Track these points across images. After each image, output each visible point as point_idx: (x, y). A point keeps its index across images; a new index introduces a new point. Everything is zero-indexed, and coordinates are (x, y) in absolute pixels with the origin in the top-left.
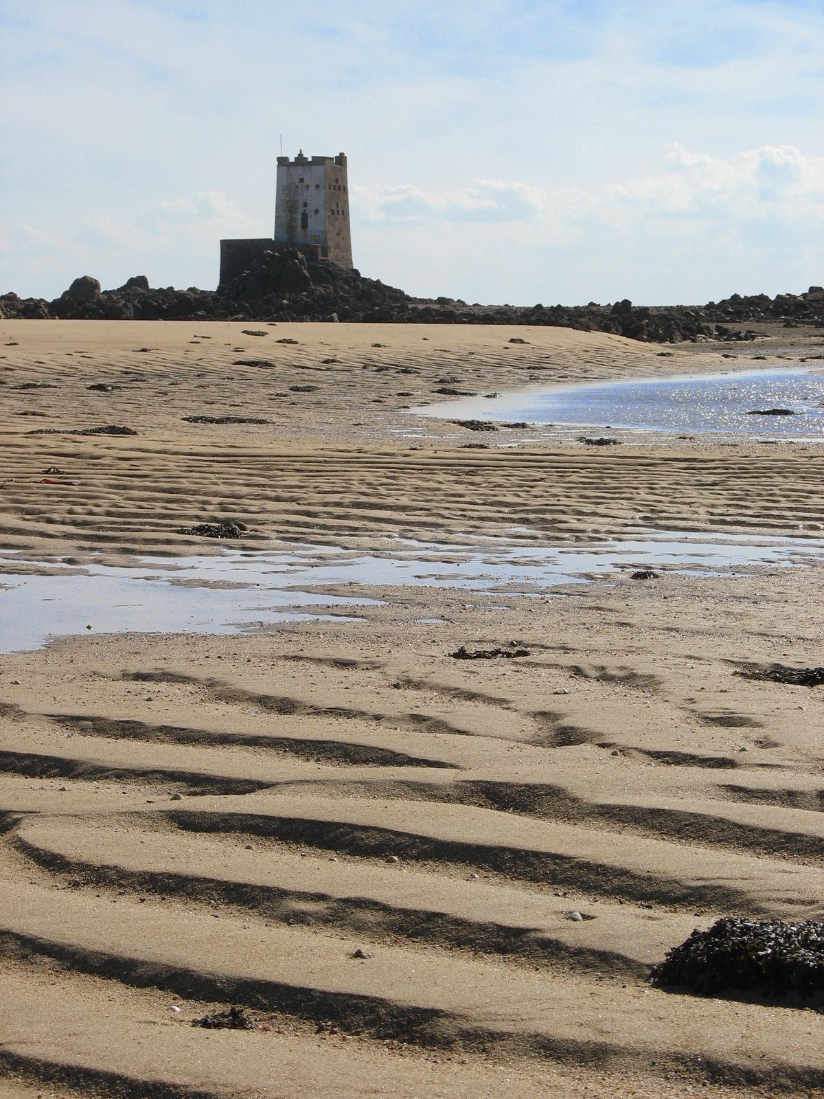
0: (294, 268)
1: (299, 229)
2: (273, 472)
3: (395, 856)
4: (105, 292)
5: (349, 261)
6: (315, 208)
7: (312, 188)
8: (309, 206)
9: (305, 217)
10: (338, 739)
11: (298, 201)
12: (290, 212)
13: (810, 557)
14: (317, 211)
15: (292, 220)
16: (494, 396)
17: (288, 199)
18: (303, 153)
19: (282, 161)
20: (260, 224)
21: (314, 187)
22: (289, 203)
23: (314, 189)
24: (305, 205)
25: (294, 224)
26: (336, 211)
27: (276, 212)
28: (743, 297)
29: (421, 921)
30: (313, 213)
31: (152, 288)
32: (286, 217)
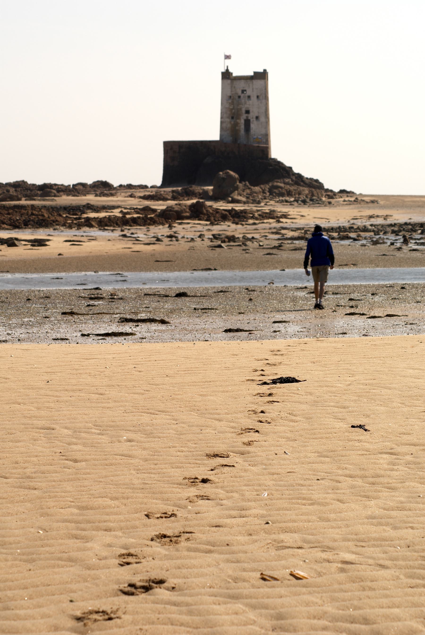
0: (227, 168)
2: (281, 524)
7: (254, 98)
9: (247, 122)
11: (241, 109)
12: (232, 118)
13: (167, 479)
14: (257, 118)
16: (60, 254)
17: (231, 107)
18: (229, 68)
19: (226, 75)
20: (206, 127)
21: (256, 97)
22: (233, 111)
23: (245, 97)
24: (248, 112)
25: (237, 128)
27: (222, 118)
28: (231, 138)
30: (255, 120)
32: (230, 122)
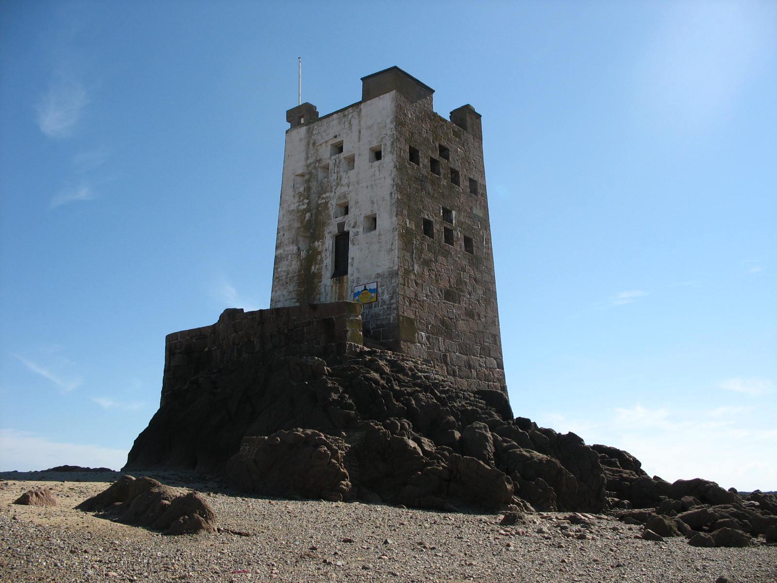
1: (327, 279)
3: (347, 394)
4: (729, 490)
5: (484, 341)
6: (369, 213)
7: (363, 160)
8: (352, 211)
9: (342, 240)
10: (352, 207)
14: (372, 222)
15: (312, 257)
26: (438, 228)
29: (316, 154)
31: (740, 491)
